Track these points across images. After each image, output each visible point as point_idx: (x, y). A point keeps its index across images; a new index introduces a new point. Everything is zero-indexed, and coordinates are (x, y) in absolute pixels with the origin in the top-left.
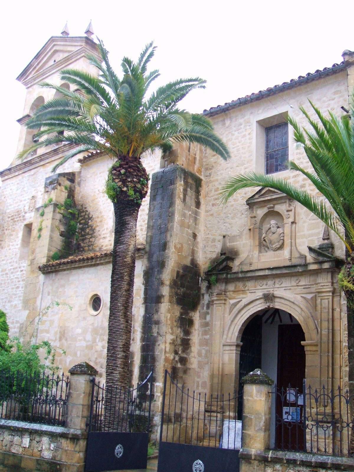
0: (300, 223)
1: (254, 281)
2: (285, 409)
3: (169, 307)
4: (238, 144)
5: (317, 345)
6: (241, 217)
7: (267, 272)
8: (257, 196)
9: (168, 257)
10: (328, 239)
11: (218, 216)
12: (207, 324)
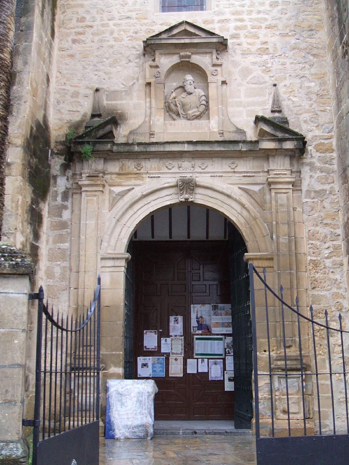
0: (232, 86)
1: (158, 160)
2: (141, 360)
3: (21, 184)
5: (272, 259)
6: (126, 65)
7: (186, 148)
8: (164, 36)
9: (20, 98)
10: (280, 112)
11: (83, 60)
12: (63, 225)
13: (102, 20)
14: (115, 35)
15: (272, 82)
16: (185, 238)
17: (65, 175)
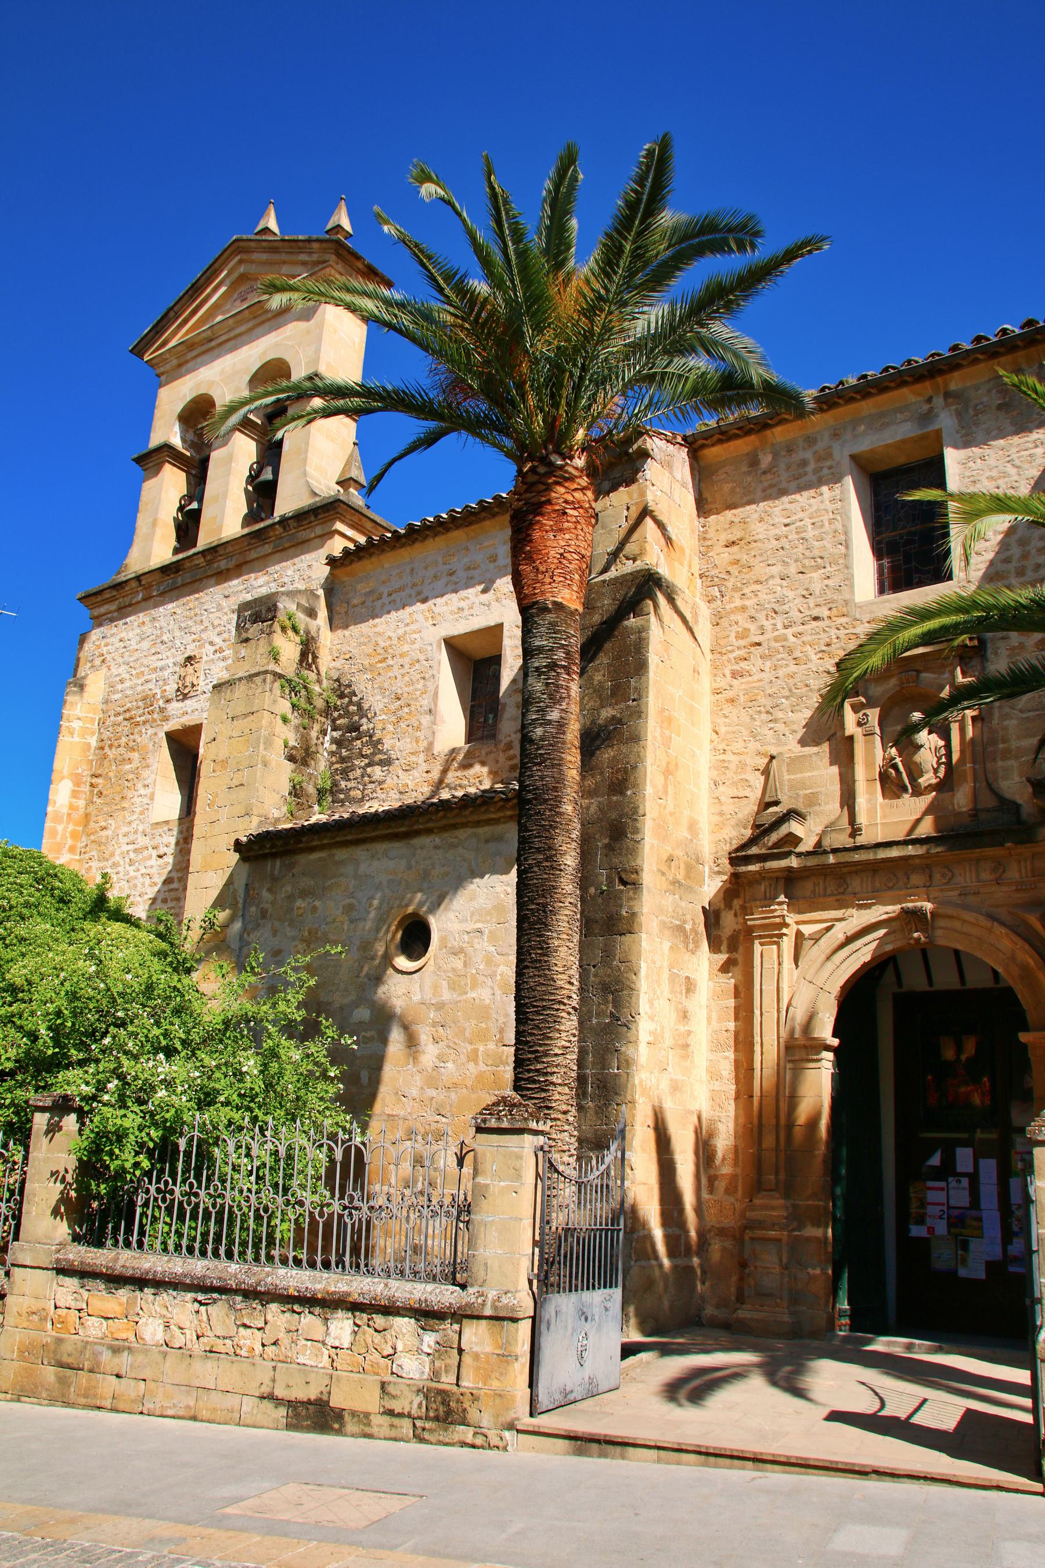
4: (800, 515)
11: (750, 704)
14: (797, 654)
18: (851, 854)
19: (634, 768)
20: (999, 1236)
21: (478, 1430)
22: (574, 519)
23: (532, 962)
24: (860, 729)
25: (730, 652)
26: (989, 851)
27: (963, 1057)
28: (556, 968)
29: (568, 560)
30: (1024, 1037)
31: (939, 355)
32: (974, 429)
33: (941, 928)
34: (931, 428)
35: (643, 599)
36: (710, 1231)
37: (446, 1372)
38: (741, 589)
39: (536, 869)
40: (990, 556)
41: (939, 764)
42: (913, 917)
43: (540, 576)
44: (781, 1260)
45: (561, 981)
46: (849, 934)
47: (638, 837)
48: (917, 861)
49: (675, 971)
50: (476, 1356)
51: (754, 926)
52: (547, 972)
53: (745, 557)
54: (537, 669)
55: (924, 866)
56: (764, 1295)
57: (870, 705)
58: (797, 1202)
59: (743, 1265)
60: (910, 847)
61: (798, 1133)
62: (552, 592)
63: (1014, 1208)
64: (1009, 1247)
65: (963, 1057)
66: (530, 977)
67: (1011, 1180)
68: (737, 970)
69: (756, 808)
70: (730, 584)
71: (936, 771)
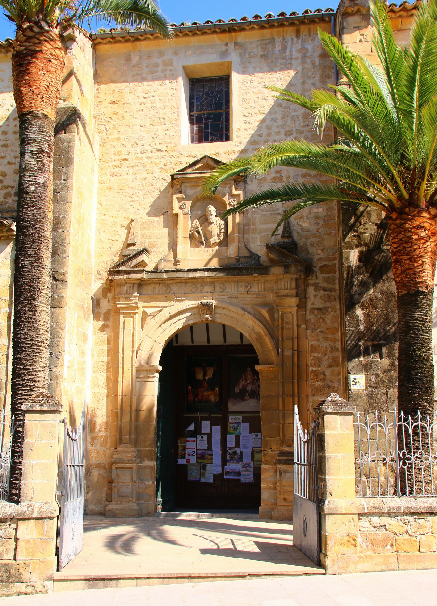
4: (153, 94)
8: (189, 171)
11: (120, 191)
13: (136, 153)
14: (148, 168)
15: (284, 209)
16: (222, 343)
17: (106, 298)
18: (175, 273)
19: (63, 217)
20: (221, 462)
21: (29, 584)
22: (55, 66)
23: (26, 319)
24: (181, 211)
25: (110, 162)
26: (244, 278)
27: (207, 378)
28: (40, 323)
29: (51, 90)
30: (257, 367)
31: (235, 20)
32: (248, 65)
33: (218, 313)
34: (227, 60)
35: (71, 124)
36: (91, 466)
37: (7, 553)
38: (118, 129)
39: (29, 266)
40: (253, 132)
41: (221, 233)
42: (207, 307)
43: (35, 97)
44: (132, 478)
45: (42, 330)
46: (171, 314)
47: (65, 255)
48: (208, 280)
49: (79, 329)
50: (28, 541)
51: (121, 307)
52: (35, 325)
53: (121, 111)
54: (31, 151)
55: (212, 282)
56: (123, 496)
57: (187, 198)
58: (140, 449)
59: (111, 482)
60: (206, 272)
61: (143, 414)
62: (41, 107)
63: (228, 449)
64: (225, 467)
65: (207, 378)
66: (25, 327)
67: (227, 436)
68: (109, 330)
69: (122, 247)
70: (111, 125)
71: (219, 236)
